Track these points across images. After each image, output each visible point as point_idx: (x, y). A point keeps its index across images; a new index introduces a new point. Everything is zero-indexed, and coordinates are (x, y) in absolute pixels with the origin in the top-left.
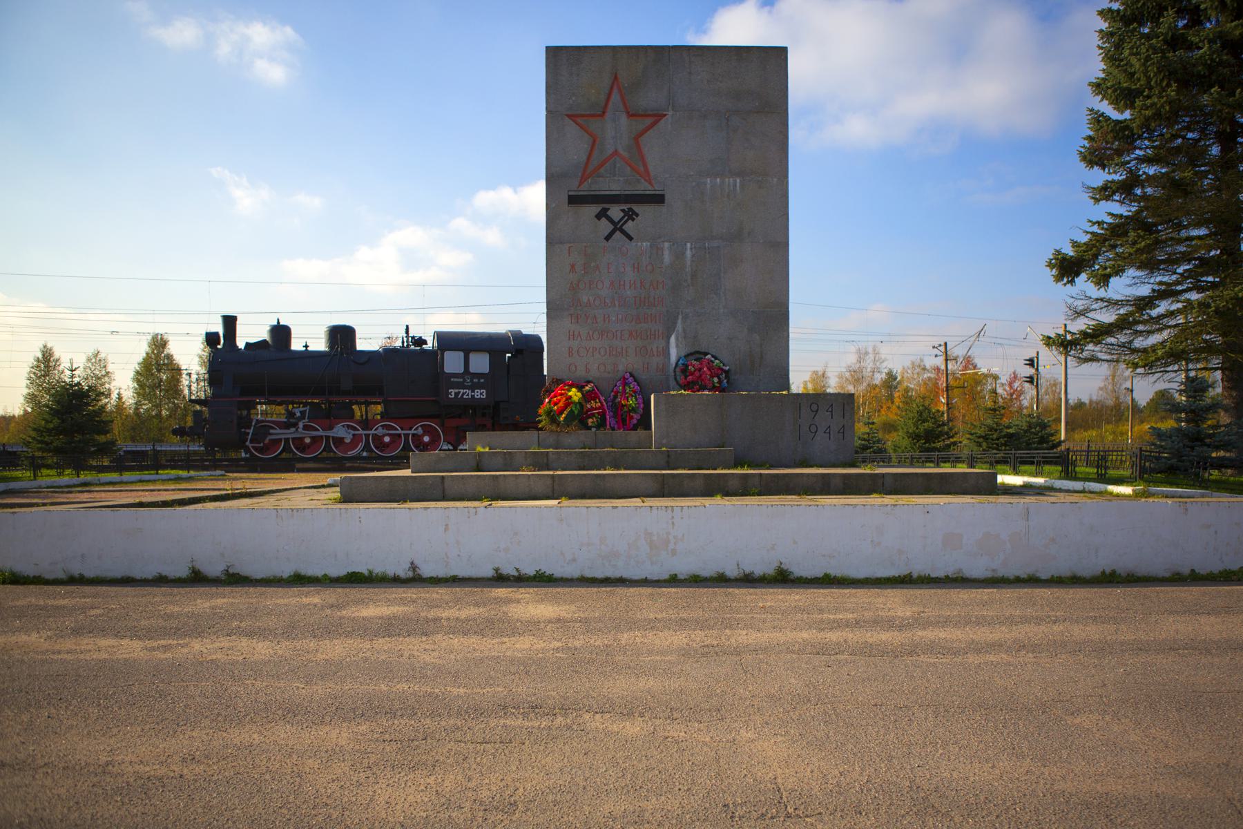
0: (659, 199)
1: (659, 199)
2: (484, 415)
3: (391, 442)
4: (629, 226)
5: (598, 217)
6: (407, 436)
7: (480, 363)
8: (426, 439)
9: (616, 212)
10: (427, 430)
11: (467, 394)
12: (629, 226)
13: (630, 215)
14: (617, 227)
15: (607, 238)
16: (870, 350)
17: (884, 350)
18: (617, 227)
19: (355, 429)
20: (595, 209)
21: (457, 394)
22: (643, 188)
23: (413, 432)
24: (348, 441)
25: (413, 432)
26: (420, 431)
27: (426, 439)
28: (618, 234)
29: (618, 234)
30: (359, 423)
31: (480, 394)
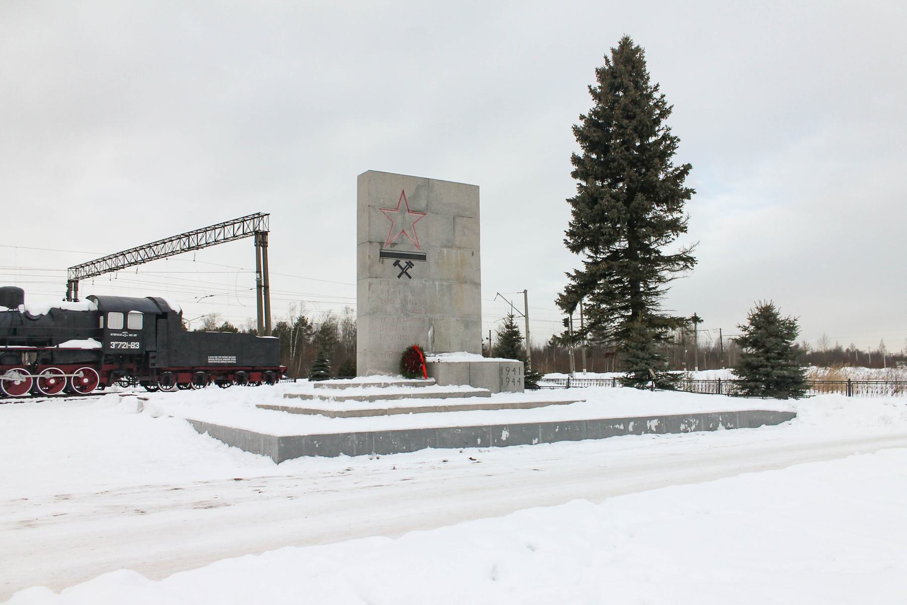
0: (423, 258)
1: (423, 258)
2: (131, 361)
3: (57, 383)
4: (409, 271)
5: (395, 265)
6: (69, 378)
7: (136, 322)
8: (86, 381)
9: (403, 263)
10: (87, 373)
11: (125, 345)
12: (409, 271)
13: (410, 265)
14: (404, 272)
15: (399, 277)
16: (298, 304)
17: (308, 306)
18: (404, 272)
19: (24, 373)
20: (393, 260)
21: (117, 345)
22: (416, 251)
23: (74, 375)
24: (17, 383)
25: (74, 375)
26: (81, 375)
27: (86, 381)
28: (404, 275)
29: (404, 275)
30: (28, 368)
31: (135, 346)
